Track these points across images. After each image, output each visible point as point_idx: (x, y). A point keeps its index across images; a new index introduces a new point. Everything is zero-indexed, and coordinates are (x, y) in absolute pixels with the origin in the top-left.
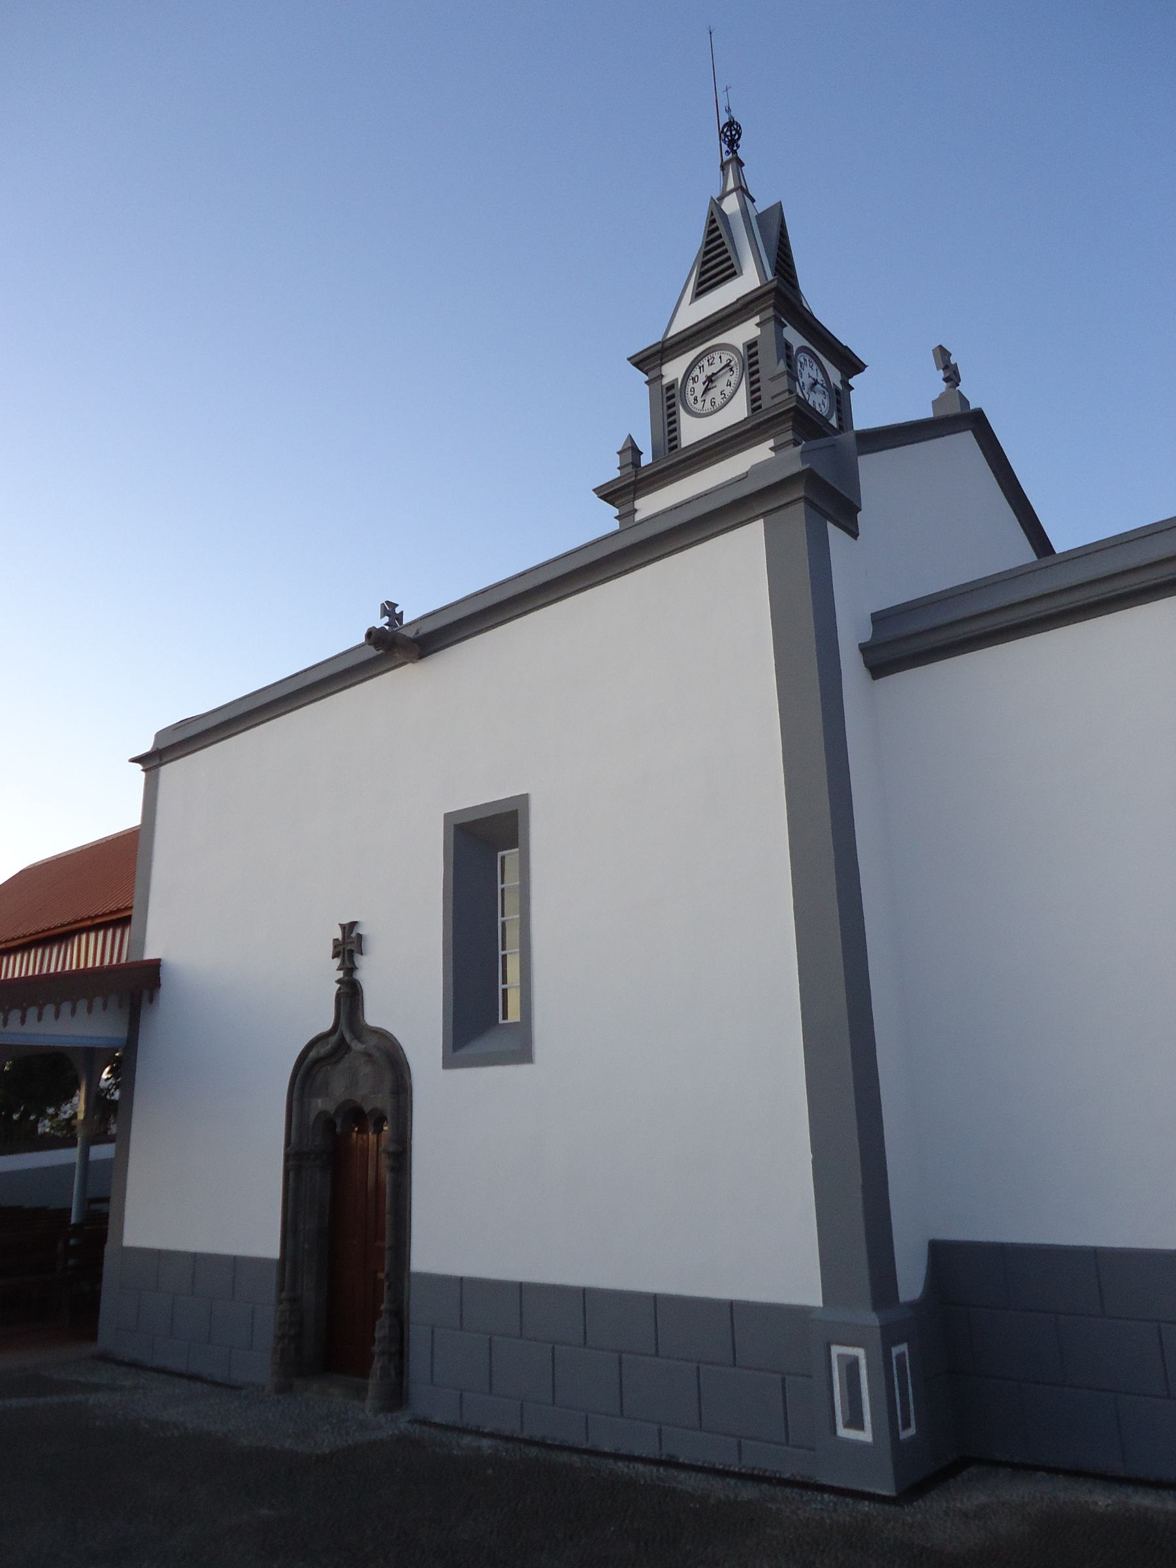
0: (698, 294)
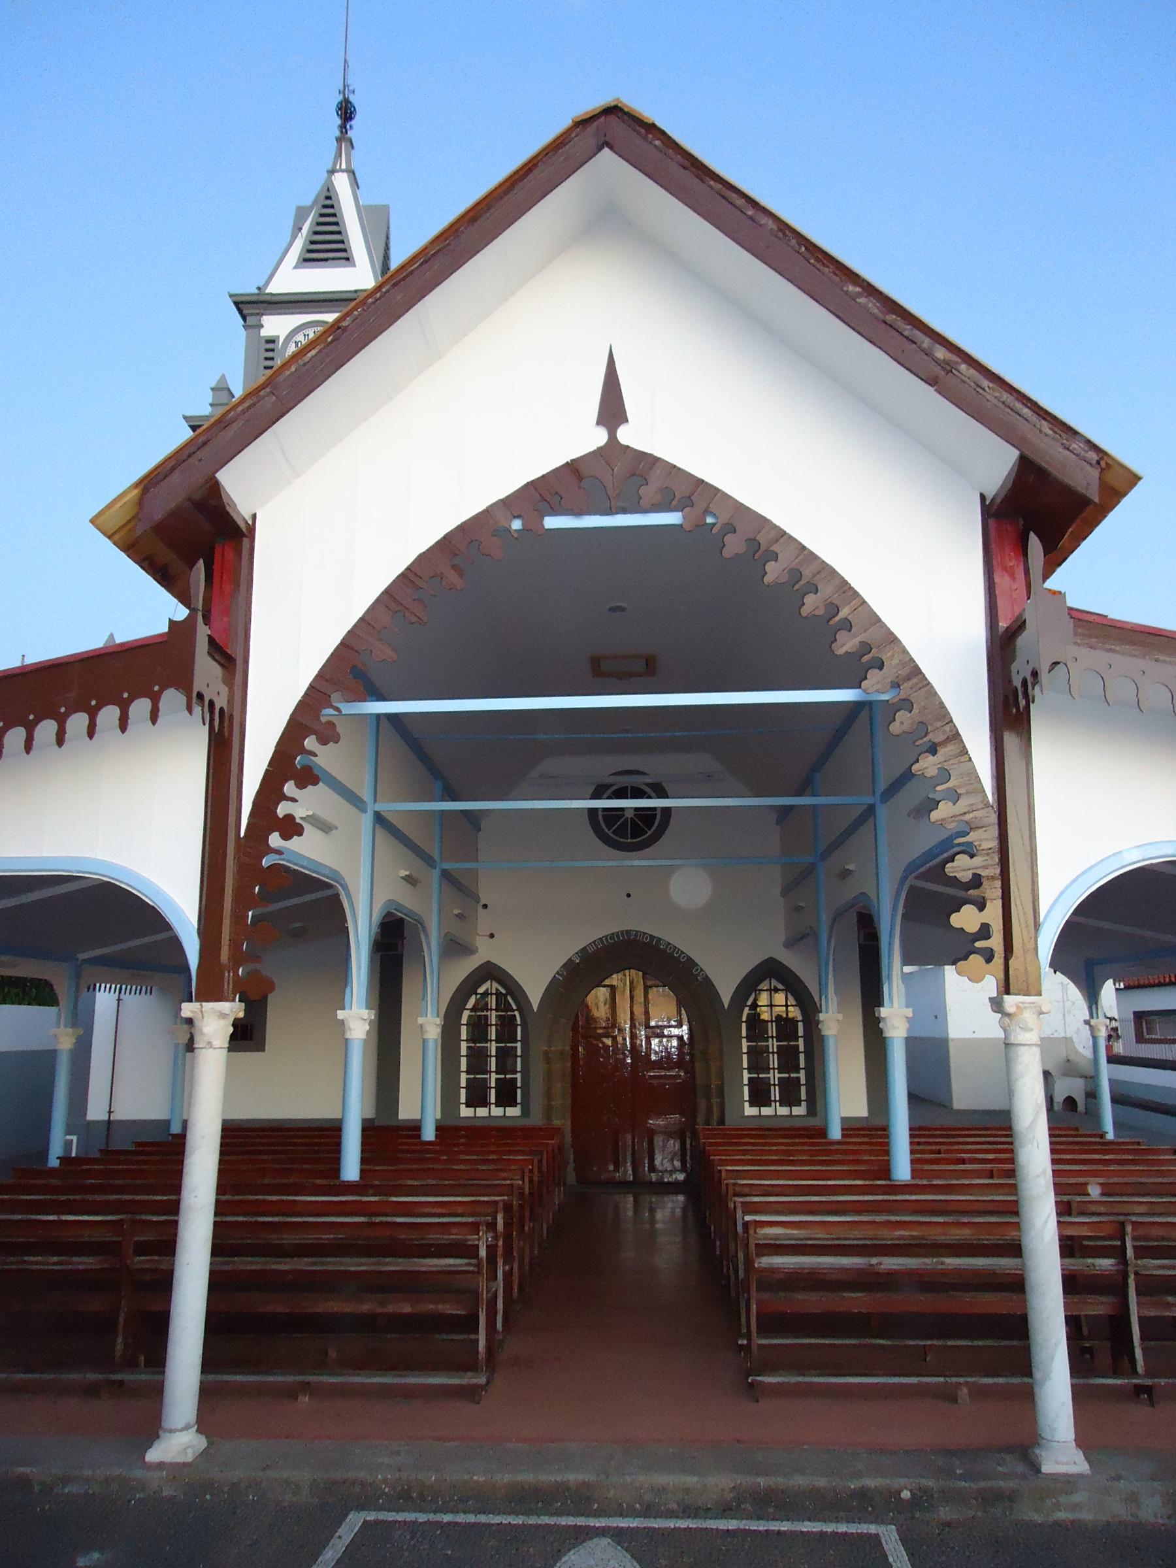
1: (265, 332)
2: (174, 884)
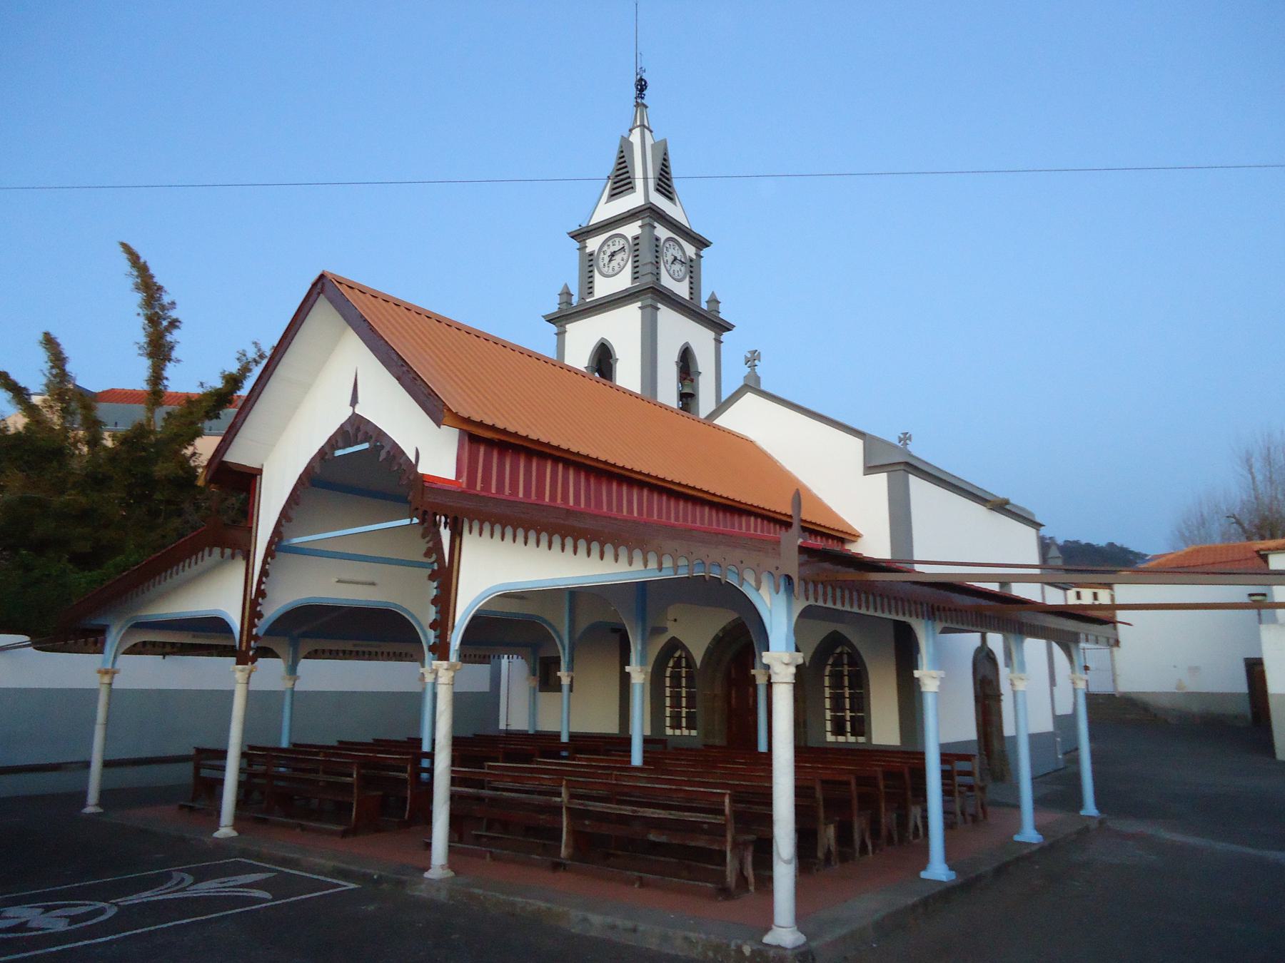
0: (613, 196)
1: (588, 250)
2: (234, 618)
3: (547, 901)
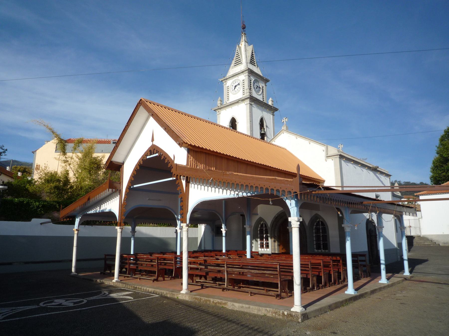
3: (221, 299)
